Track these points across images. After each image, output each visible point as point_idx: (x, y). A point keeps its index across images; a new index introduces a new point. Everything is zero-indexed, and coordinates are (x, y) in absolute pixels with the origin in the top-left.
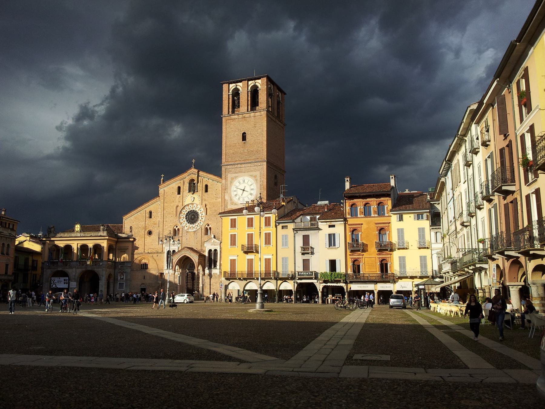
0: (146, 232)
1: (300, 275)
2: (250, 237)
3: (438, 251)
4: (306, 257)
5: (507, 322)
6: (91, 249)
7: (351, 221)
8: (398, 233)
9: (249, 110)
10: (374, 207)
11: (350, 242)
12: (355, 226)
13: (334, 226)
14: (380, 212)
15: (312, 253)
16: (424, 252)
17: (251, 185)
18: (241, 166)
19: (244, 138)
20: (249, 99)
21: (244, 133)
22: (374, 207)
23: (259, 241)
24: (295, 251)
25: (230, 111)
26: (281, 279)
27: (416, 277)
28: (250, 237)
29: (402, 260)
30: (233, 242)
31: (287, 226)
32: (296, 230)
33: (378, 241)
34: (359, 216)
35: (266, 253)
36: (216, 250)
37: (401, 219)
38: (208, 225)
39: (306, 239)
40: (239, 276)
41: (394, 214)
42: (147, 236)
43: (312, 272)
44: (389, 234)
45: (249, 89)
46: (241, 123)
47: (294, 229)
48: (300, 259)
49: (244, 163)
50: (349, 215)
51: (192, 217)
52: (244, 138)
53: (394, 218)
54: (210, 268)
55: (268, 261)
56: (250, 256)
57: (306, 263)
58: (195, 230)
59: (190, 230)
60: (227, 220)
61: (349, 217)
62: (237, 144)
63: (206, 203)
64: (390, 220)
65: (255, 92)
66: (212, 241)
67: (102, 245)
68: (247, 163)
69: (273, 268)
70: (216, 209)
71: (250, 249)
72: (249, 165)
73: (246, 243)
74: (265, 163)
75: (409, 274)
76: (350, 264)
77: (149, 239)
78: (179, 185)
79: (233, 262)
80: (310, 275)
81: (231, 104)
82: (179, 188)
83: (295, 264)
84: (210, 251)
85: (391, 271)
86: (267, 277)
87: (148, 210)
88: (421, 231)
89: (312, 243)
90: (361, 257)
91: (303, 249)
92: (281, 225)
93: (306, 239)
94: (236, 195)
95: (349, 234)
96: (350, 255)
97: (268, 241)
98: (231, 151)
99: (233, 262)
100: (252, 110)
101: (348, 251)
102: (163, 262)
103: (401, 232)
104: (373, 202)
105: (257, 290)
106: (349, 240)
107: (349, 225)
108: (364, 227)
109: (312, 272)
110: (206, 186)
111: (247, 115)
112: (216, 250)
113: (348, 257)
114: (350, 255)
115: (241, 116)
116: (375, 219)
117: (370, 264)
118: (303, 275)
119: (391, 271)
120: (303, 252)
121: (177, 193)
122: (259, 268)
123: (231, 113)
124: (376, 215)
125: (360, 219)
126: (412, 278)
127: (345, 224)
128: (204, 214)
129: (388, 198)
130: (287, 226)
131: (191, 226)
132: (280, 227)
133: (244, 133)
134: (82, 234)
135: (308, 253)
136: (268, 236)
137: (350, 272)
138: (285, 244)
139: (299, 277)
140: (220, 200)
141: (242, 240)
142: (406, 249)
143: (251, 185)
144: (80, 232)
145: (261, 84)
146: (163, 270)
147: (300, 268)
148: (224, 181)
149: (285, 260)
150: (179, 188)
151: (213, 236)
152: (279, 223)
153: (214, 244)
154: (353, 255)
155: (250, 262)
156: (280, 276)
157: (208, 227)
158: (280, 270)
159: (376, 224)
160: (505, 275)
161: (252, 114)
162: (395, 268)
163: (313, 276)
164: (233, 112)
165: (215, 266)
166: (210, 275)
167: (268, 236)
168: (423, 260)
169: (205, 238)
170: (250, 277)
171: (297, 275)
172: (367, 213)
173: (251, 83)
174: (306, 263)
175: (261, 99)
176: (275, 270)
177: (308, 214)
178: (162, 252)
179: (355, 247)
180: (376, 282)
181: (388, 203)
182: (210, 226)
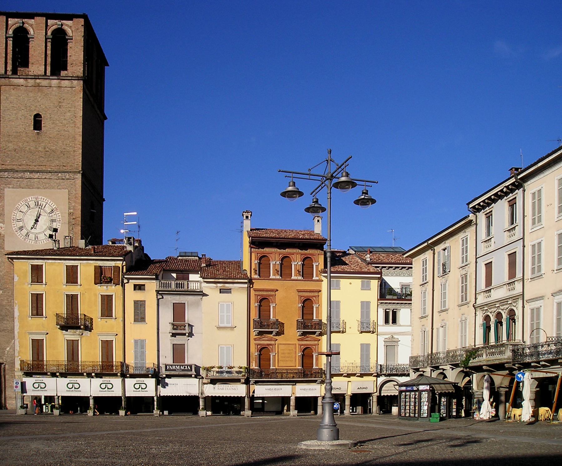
1: (170, 370)
2: (72, 300)
3: (387, 337)
4: (179, 340)
7: (258, 285)
9: (48, 73)
10: (296, 263)
11: (257, 318)
12: (265, 293)
13: (228, 291)
14: (306, 272)
15: (191, 335)
16: (368, 338)
18: (32, 176)
19: (37, 124)
20: (49, 52)
22: (296, 263)
23: (89, 307)
24: (158, 329)
25: (10, 68)
26: (133, 376)
27: (354, 375)
28: (72, 300)
33: (300, 319)
34: (272, 277)
35: (104, 329)
39: (179, 311)
40: (89, 369)
43: (191, 366)
44: (317, 308)
45: (49, 33)
46: (31, 94)
47: (157, 292)
48: (167, 343)
49: (38, 172)
50: (256, 274)
52: (37, 124)
55: (107, 346)
56: (71, 335)
57: (179, 352)
60: (24, 267)
61: (257, 276)
62: (24, 135)
64: (321, 286)
65: (59, 41)
68: (42, 172)
69: (117, 358)
71: (72, 322)
72: (48, 176)
73: (63, 310)
74: (79, 176)
75: (344, 371)
76: (255, 353)
79: (37, 346)
80: (188, 370)
83: (158, 351)
85: (317, 365)
88: (365, 306)
89: (190, 316)
90: (273, 342)
91: (175, 326)
93: (179, 311)
94: (21, 228)
95: (254, 305)
96: (255, 339)
97: (107, 311)
98: (11, 146)
99: (37, 346)
100: (53, 74)
101: (253, 333)
104: (296, 258)
105: (153, 397)
106: (254, 315)
107: (256, 290)
109: (191, 366)
111: (44, 83)
113: (253, 342)
114: (255, 339)
115: (31, 82)
118: (174, 370)
119: (317, 365)
120: (174, 331)
122: (90, 353)
123: (9, 73)
124: (300, 278)
125: (272, 282)
127: (249, 289)
129: (319, 251)
132: (129, 287)
135: (185, 334)
137: (254, 366)
138: (140, 317)
139: (168, 373)
141: (55, 306)
142: (343, 332)
145: (74, 30)
147: (167, 358)
149: (140, 344)
152: (128, 279)
154: (259, 339)
155: (73, 349)
156: (131, 371)
158: (130, 360)
159: (299, 291)
160: (308, 345)
161: (55, 82)
163: (193, 372)
164: (15, 72)
167: (107, 301)
168: (365, 348)
170: (72, 370)
171: (164, 369)
172: (284, 271)
173: (54, 24)
174: (179, 352)
175: (73, 58)
176: (122, 360)
177: (174, 271)
179: (263, 324)
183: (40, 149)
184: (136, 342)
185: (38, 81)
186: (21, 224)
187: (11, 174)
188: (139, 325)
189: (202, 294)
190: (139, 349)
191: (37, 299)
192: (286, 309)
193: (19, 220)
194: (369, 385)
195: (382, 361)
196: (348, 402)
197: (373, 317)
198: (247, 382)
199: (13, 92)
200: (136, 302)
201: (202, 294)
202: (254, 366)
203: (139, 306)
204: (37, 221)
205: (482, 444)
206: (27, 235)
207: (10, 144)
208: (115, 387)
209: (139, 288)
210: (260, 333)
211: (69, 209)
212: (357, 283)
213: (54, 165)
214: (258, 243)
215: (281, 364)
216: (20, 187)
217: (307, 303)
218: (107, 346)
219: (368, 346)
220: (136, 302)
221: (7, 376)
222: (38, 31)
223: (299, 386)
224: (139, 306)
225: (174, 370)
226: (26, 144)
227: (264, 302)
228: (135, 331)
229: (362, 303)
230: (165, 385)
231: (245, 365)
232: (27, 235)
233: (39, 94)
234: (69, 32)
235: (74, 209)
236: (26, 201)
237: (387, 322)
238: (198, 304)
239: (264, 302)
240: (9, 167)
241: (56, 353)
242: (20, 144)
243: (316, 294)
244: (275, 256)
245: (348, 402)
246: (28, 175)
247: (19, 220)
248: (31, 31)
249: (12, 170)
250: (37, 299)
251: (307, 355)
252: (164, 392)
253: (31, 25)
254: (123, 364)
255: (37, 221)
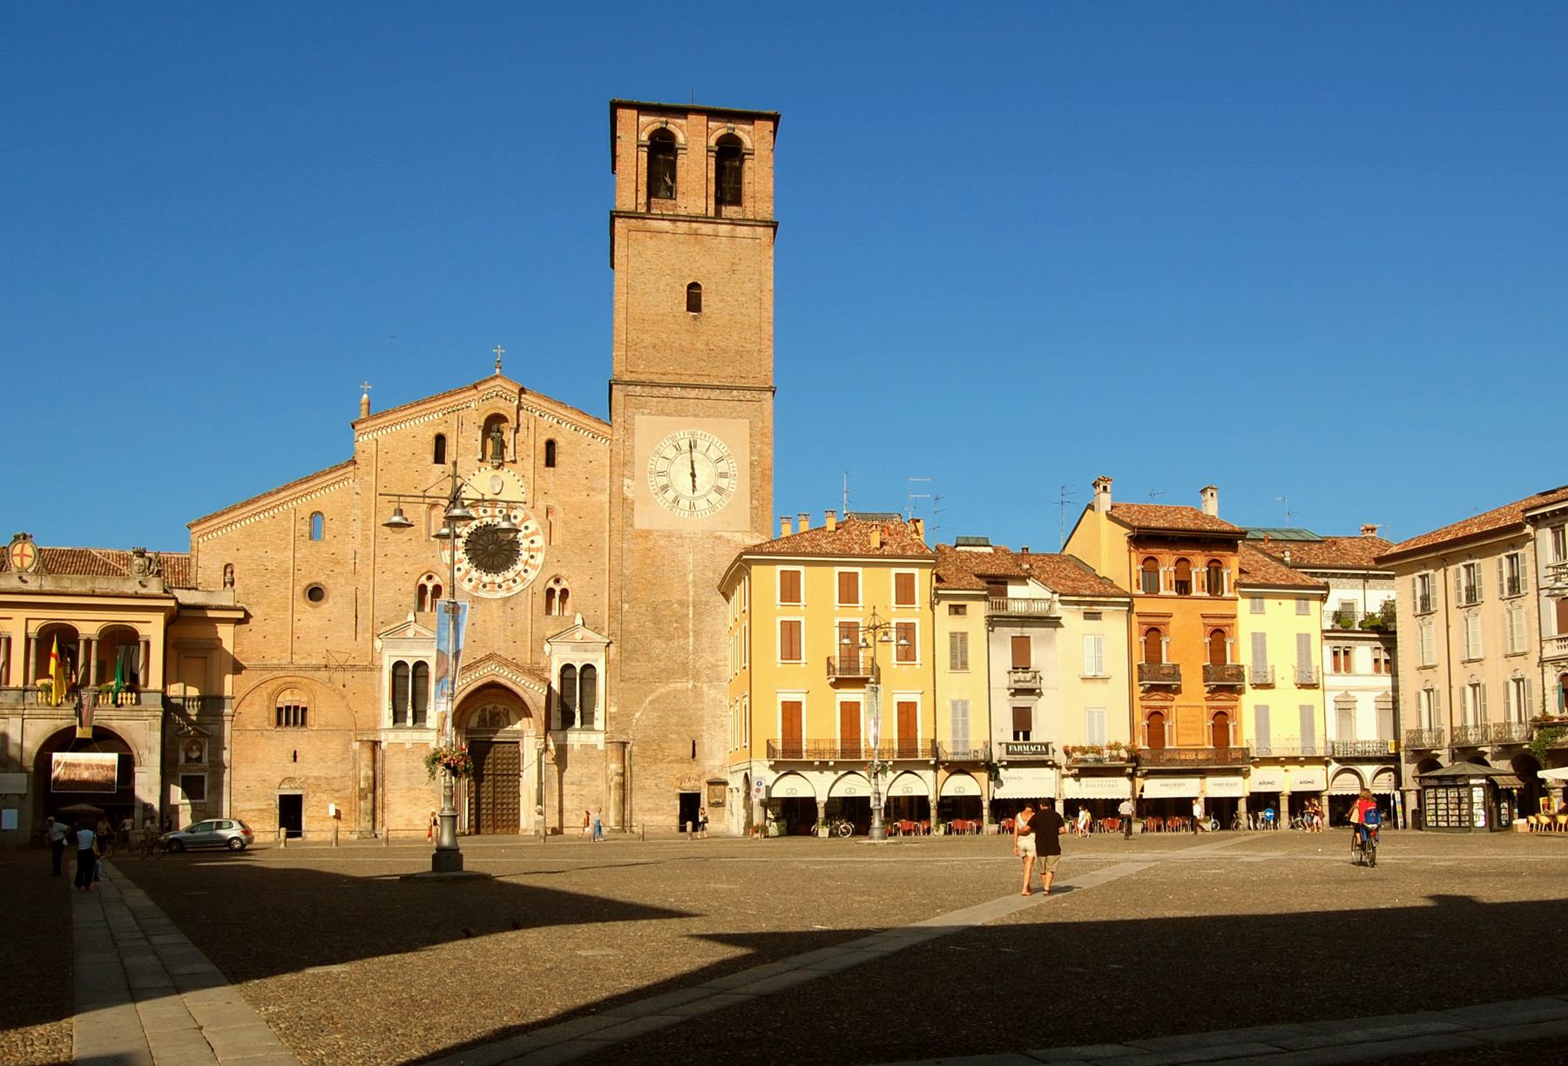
0: (299, 590)
1: (1013, 753)
5: (151, 843)
6: (88, 642)
7: (1141, 606)
8: (953, 647)
17: (720, 460)
18: (685, 393)
21: (694, 286)
29: (1262, 713)
30: (791, 650)
31: (964, 606)
32: (993, 622)
34: (1162, 592)
35: (901, 684)
36: (588, 668)
37: (1261, 610)
38: (557, 581)
41: (1244, 595)
42: (303, 605)
46: (683, 248)
51: (494, 549)
53: (1244, 605)
54: (568, 721)
55: (907, 712)
57: (1022, 721)
58: (502, 594)
59: (483, 594)
63: (551, 503)
66: (578, 636)
67: (143, 630)
70: (590, 528)
76: (1142, 722)
77: (310, 617)
78: (441, 430)
79: (792, 712)
80: (1041, 753)
81: (643, 179)
82: (440, 440)
84: (567, 668)
86: (907, 761)
87: (305, 506)
88: (1303, 640)
92: (945, 605)
95: (1139, 639)
96: (1141, 699)
99: (792, 712)
101: (1138, 691)
102: (376, 701)
103: (1259, 640)
106: (1139, 658)
107: (1139, 615)
108: (1175, 624)
110: (550, 445)
111: (706, 228)
112: (588, 668)
116: (1199, 604)
117: (1188, 726)
118: (1021, 753)
121: (431, 458)
122: (878, 731)
126: (824, 766)
127: (1130, 611)
128: (540, 541)
130: (964, 606)
131: (487, 578)
133: (694, 286)
134: (48, 584)
136: (907, 631)
137: (1142, 744)
138: (959, 661)
139: (1012, 758)
140: (605, 498)
141: (821, 644)
143: (720, 460)
144: (36, 572)
146: (375, 730)
147: (1004, 730)
148: (619, 434)
149: (960, 708)
150: (440, 440)
151: (579, 621)
153: (583, 645)
155: (850, 713)
157: (558, 589)
159: (1204, 616)
162: (1246, 734)
165: (588, 719)
166: (562, 751)
168: (1306, 713)
169: (549, 627)
170: (850, 759)
174: (1022, 721)
178: (372, 668)
179: (1156, 681)
180: (1201, 773)
181: (922, 579)
182: (564, 584)
183: (699, 345)
184: (954, 704)
185: (694, 225)
186: (664, 481)
187: (647, 390)
188: (958, 677)
189: (1055, 622)
190: (960, 717)
191: (791, 632)
192: (1185, 649)
193: (661, 474)
194: (1313, 778)
195: (1333, 735)
196: (1284, 806)
197: (1315, 660)
198: (1132, 777)
199: (650, 243)
200: (953, 635)
201: (1055, 622)
202: (1142, 744)
203: (959, 642)
204: (693, 475)
205: (561, 443)
206: (692, 506)
207: (644, 336)
208: (922, 784)
209: (957, 610)
210: (1147, 691)
211: (752, 454)
212: (1292, 603)
213: (724, 375)
214: (1143, 538)
215: (1183, 741)
216: (663, 413)
217: (1219, 636)
218: (907, 712)
219: (1311, 708)
220: (953, 635)
221: (635, 768)
222: (695, 141)
223: (1210, 781)
224: (959, 642)
225: (1021, 753)
226: (673, 336)
227: (1153, 633)
228: (952, 686)
229: (1299, 636)
230: (999, 784)
231: (1125, 740)
232: (692, 506)
233: (697, 248)
234: (748, 143)
235: (760, 455)
236: (673, 438)
237: (1337, 668)
238: (1051, 639)
239: (1153, 633)
240: (643, 378)
241: (823, 729)
242: (664, 336)
243: (1229, 621)
244: (1167, 562)
245: (1284, 806)
246: (677, 392)
247: (661, 474)
248: (681, 139)
249: (653, 385)
250: (791, 632)
251: (1221, 722)
252: (1001, 794)
253: (680, 127)
254: (935, 749)
255: (693, 475)
